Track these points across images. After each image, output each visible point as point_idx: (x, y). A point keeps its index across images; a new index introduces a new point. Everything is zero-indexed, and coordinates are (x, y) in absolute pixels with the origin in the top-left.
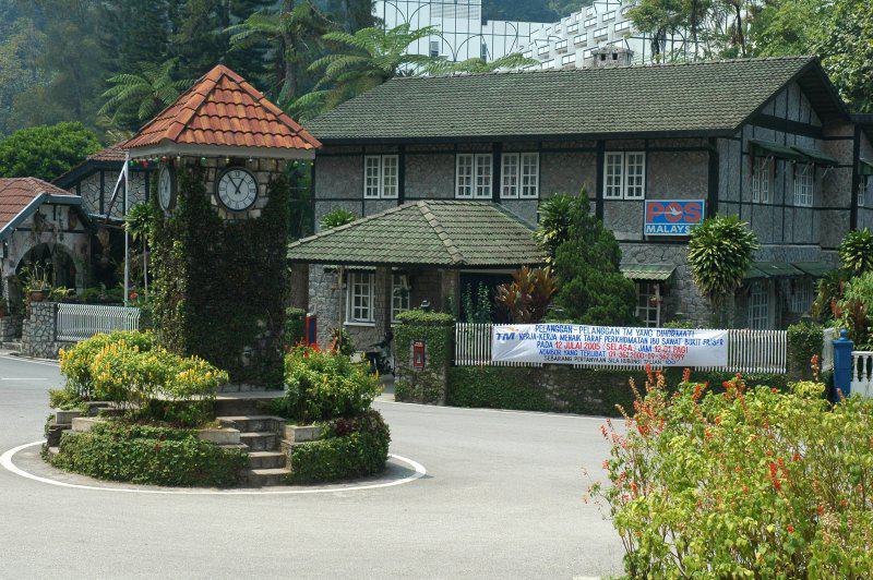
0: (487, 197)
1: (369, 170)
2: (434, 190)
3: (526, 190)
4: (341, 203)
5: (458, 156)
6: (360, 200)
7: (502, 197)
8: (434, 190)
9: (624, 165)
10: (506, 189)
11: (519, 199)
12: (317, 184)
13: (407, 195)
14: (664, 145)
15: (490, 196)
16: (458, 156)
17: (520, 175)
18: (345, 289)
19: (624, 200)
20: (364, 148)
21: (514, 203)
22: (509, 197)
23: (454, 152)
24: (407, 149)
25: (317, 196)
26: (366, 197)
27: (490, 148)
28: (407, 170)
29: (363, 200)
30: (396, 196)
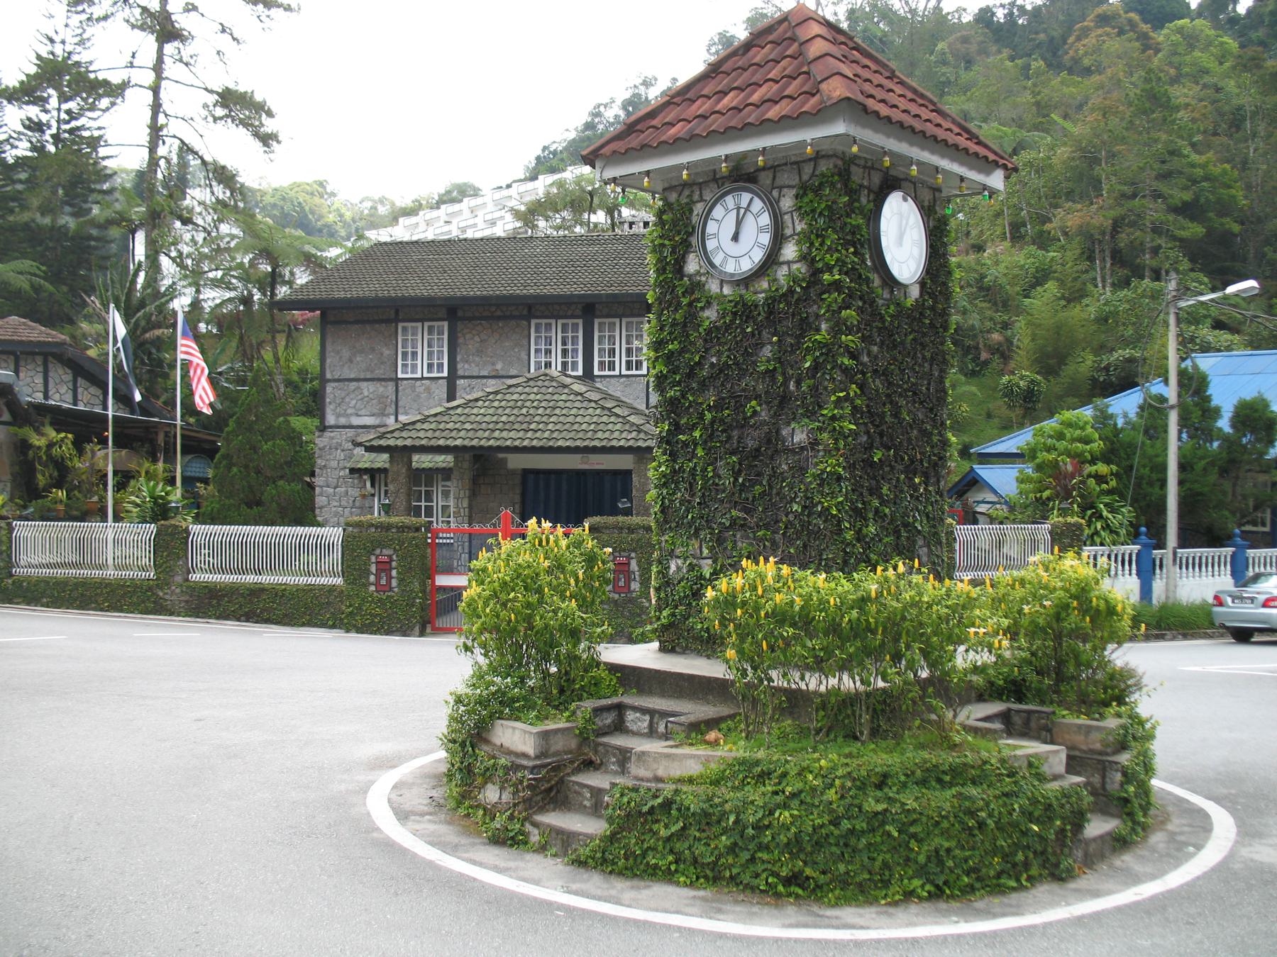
0: (440, 375)
1: (405, 341)
2: (499, 366)
3: (430, 366)
4: (365, 384)
5: (533, 322)
6: (391, 380)
7: (596, 372)
8: (499, 366)
9: (557, 335)
10: (601, 364)
11: (423, 378)
12: (328, 361)
13: (460, 373)
14: (499, 313)
15: (580, 373)
16: (400, 325)
17: (422, 350)
18: (373, 495)
19: (621, 376)
20: (397, 312)
21: (613, 380)
22: (607, 373)
23: (528, 318)
24: (460, 314)
25: (328, 376)
26: (400, 375)
27: (578, 312)
28: (461, 340)
29: (397, 380)
30: (445, 374)
